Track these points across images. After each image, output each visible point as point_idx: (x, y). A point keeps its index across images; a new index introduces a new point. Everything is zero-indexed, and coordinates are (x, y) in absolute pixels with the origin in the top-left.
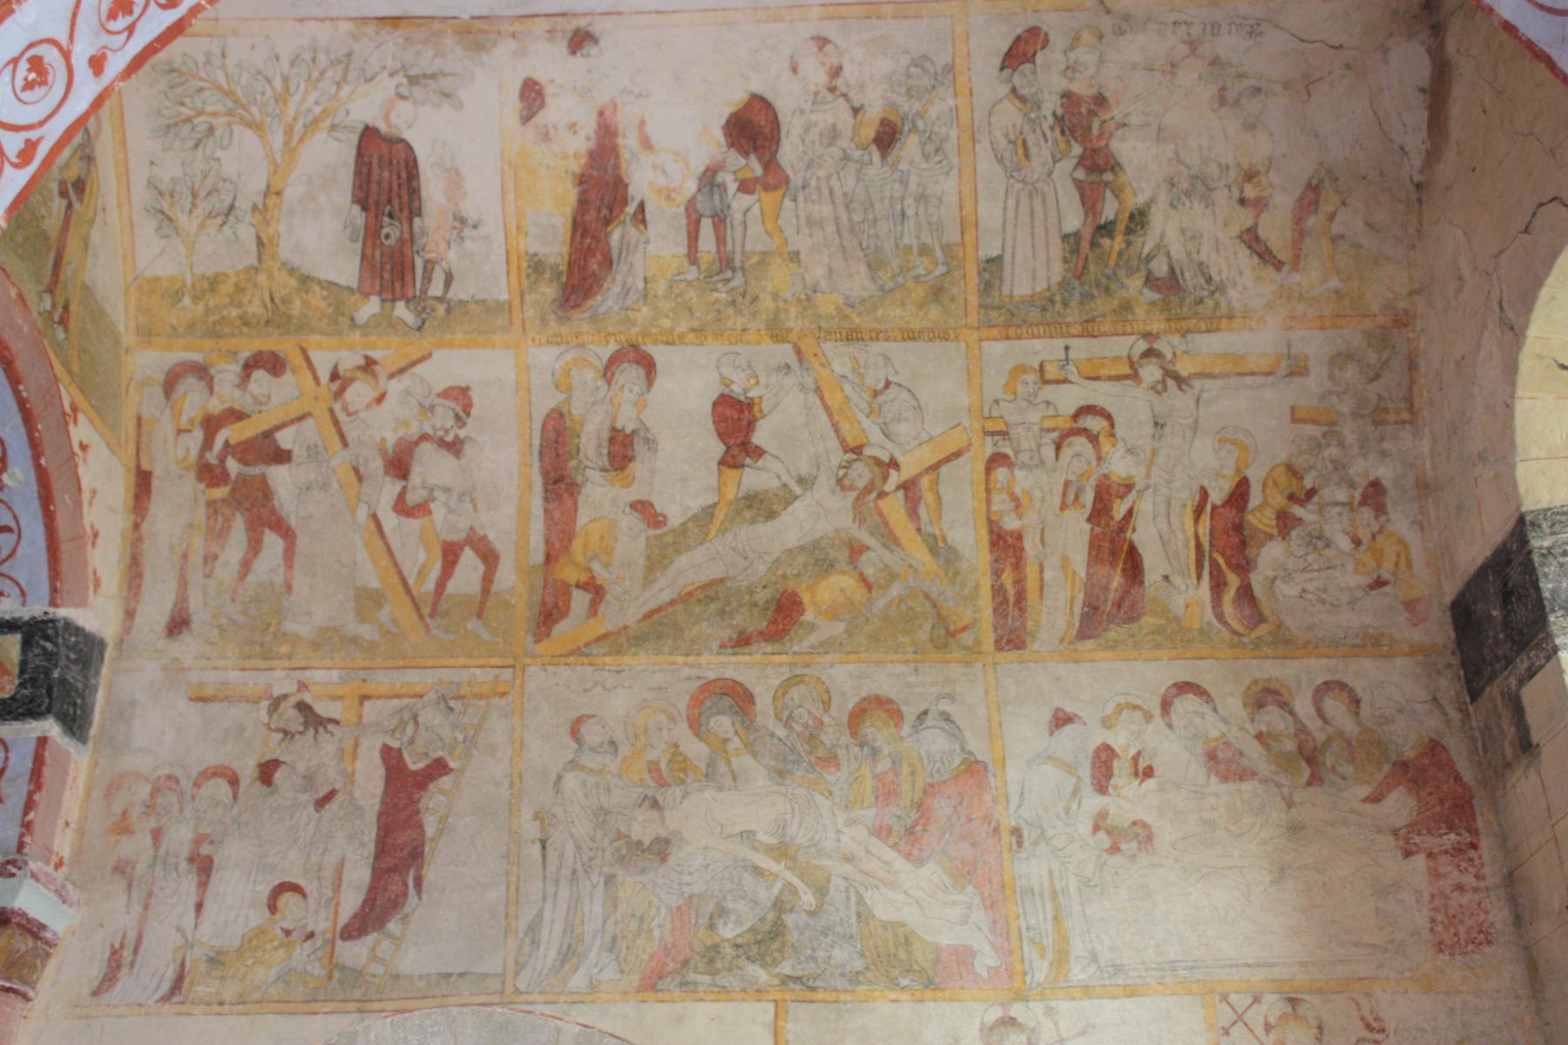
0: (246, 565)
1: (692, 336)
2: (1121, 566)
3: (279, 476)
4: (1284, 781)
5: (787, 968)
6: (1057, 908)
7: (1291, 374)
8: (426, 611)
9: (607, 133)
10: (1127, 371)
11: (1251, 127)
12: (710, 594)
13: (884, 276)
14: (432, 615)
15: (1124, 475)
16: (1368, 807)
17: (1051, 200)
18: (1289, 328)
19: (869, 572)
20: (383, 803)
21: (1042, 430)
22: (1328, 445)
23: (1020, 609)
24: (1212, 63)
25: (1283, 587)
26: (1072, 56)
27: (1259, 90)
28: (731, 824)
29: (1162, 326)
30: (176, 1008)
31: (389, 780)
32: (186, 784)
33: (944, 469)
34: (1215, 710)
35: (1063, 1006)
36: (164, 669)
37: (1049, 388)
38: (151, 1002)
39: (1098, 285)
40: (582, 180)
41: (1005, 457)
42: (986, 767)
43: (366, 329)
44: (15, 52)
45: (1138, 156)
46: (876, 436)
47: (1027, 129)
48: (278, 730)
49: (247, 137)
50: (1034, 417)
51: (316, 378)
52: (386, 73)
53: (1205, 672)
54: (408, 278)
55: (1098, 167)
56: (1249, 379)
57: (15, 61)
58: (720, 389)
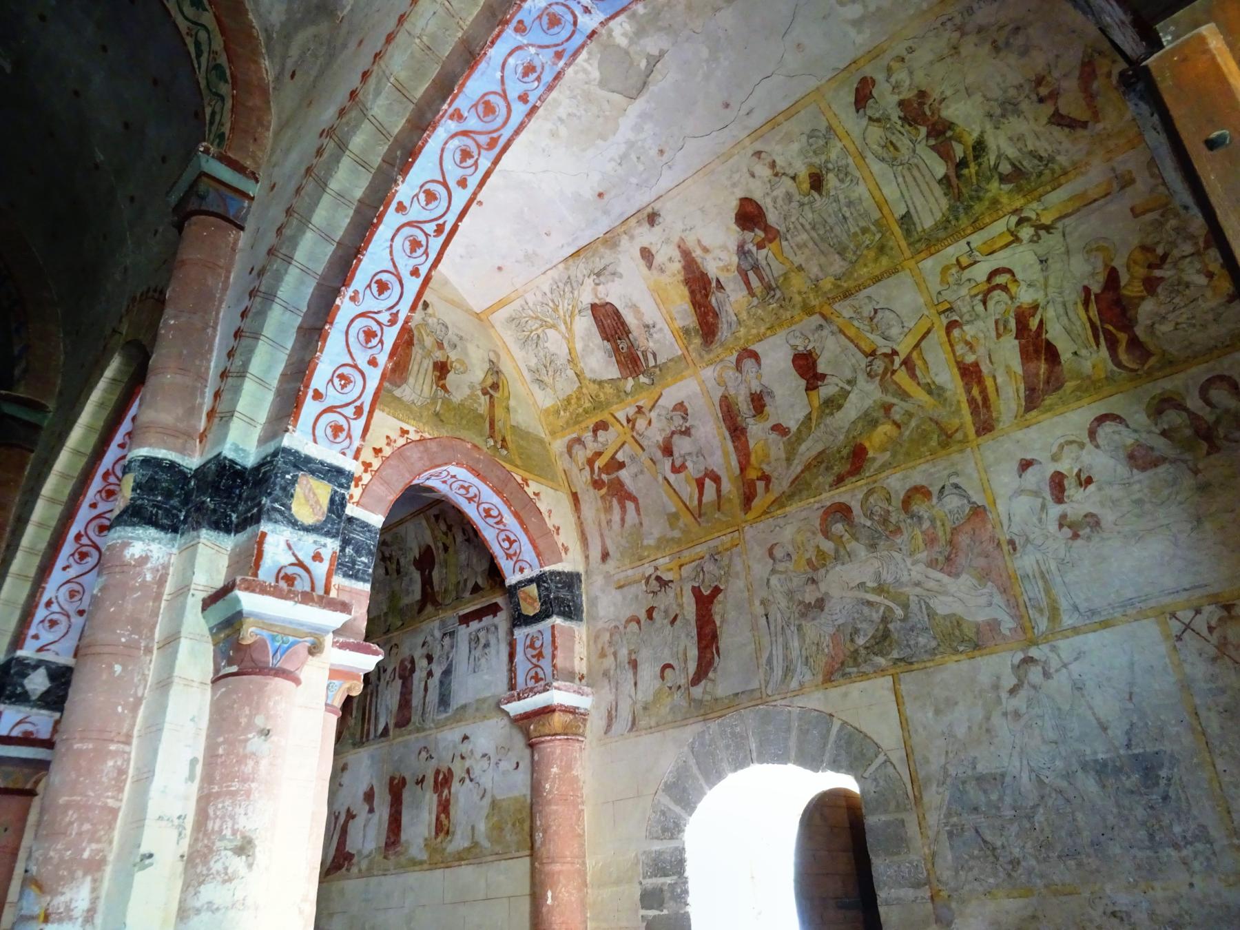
0: (623, 520)
1: (769, 333)
3: (624, 474)
5: (895, 654)
6: (1046, 582)
7: (1123, 188)
9: (686, 255)
11: (1025, 52)
12: (820, 461)
13: (850, 255)
17: (922, 166)
18: (1109, 160)
19: (897, 417)
22: (1168, 220)
24: (979, 32)
26: (893, 80)
28: (853, 575)
33: (923, 344)
35: (1062, 644)
39: (971, 198)
40: (687, 282)
41: (956, 321)
44: (329, 377)
45: (964, 114)
46: (880, 342)
47: (889, 135)
49: (551, 333)
55: (941, 133)
56: (1095, 205)
57: (331, 380)
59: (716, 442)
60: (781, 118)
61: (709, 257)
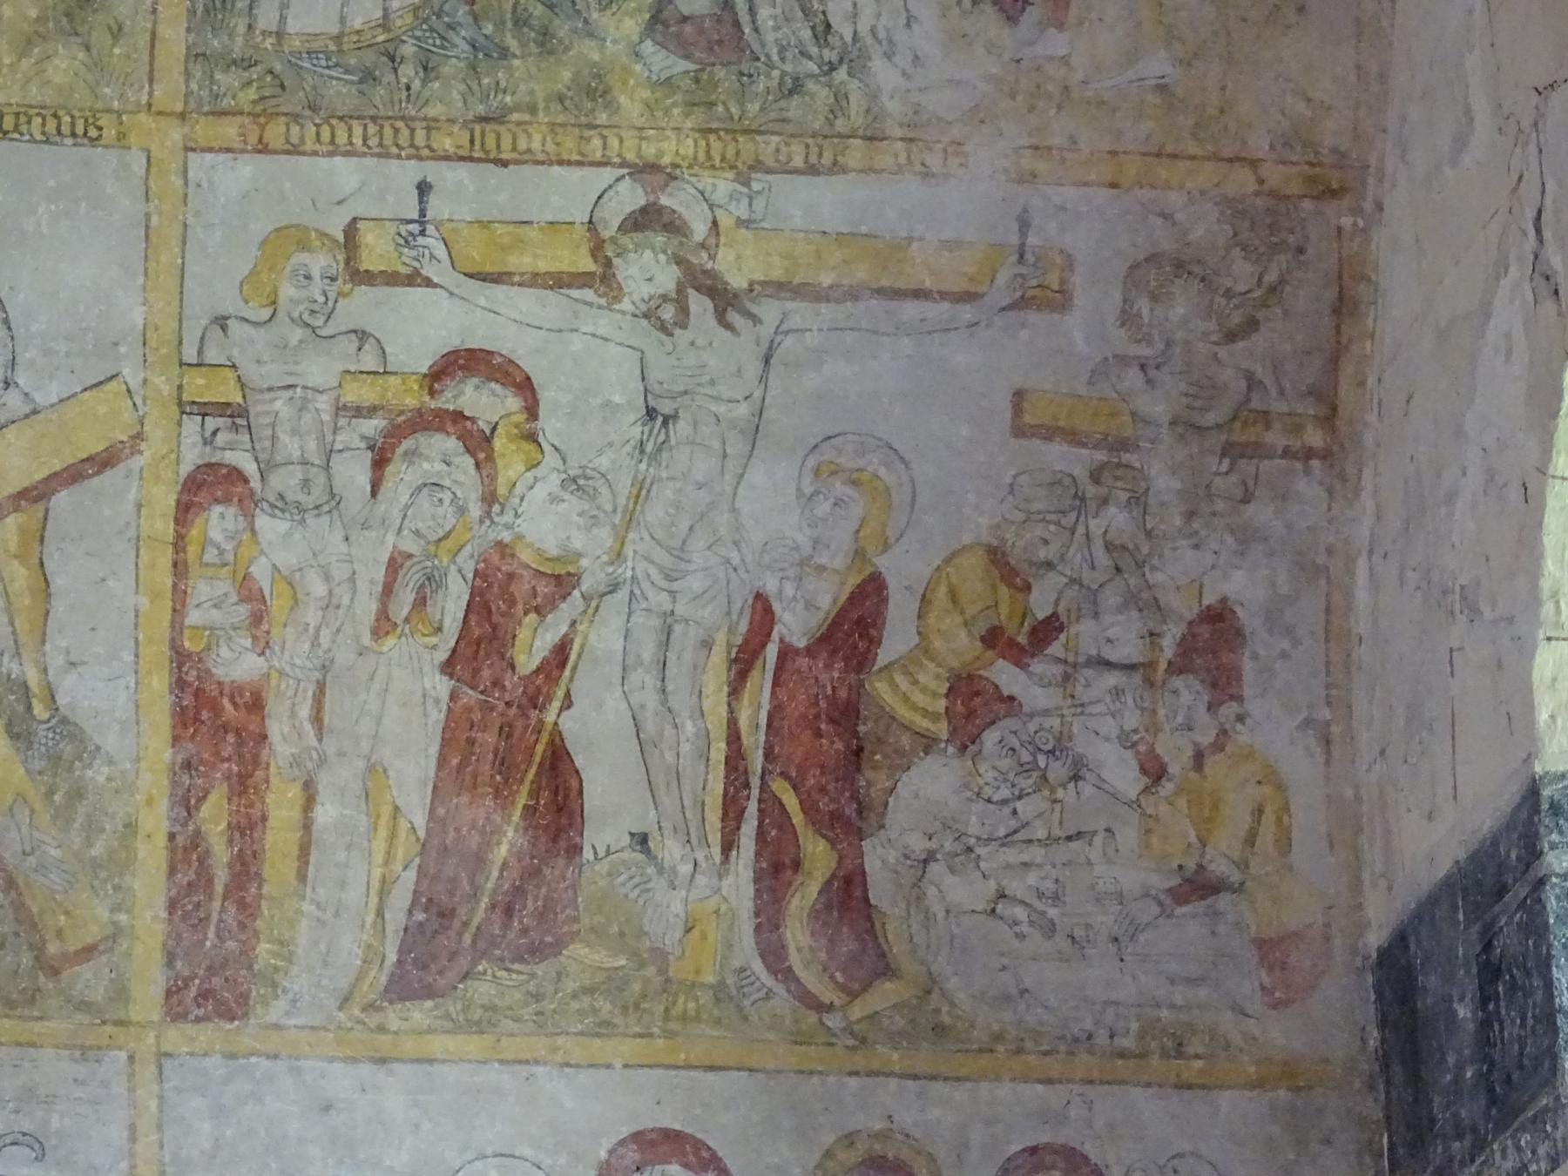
2: (522, 800)
7: (1022, 304)
10: (587, 264)
21: (340, 409)
23: (242, 905)
25: (949, 880)
29: (688, 147)
33: (62, 499)
37: (364, 294)
39: (520, 22)
41: (237, 475)
56: (910, 310)
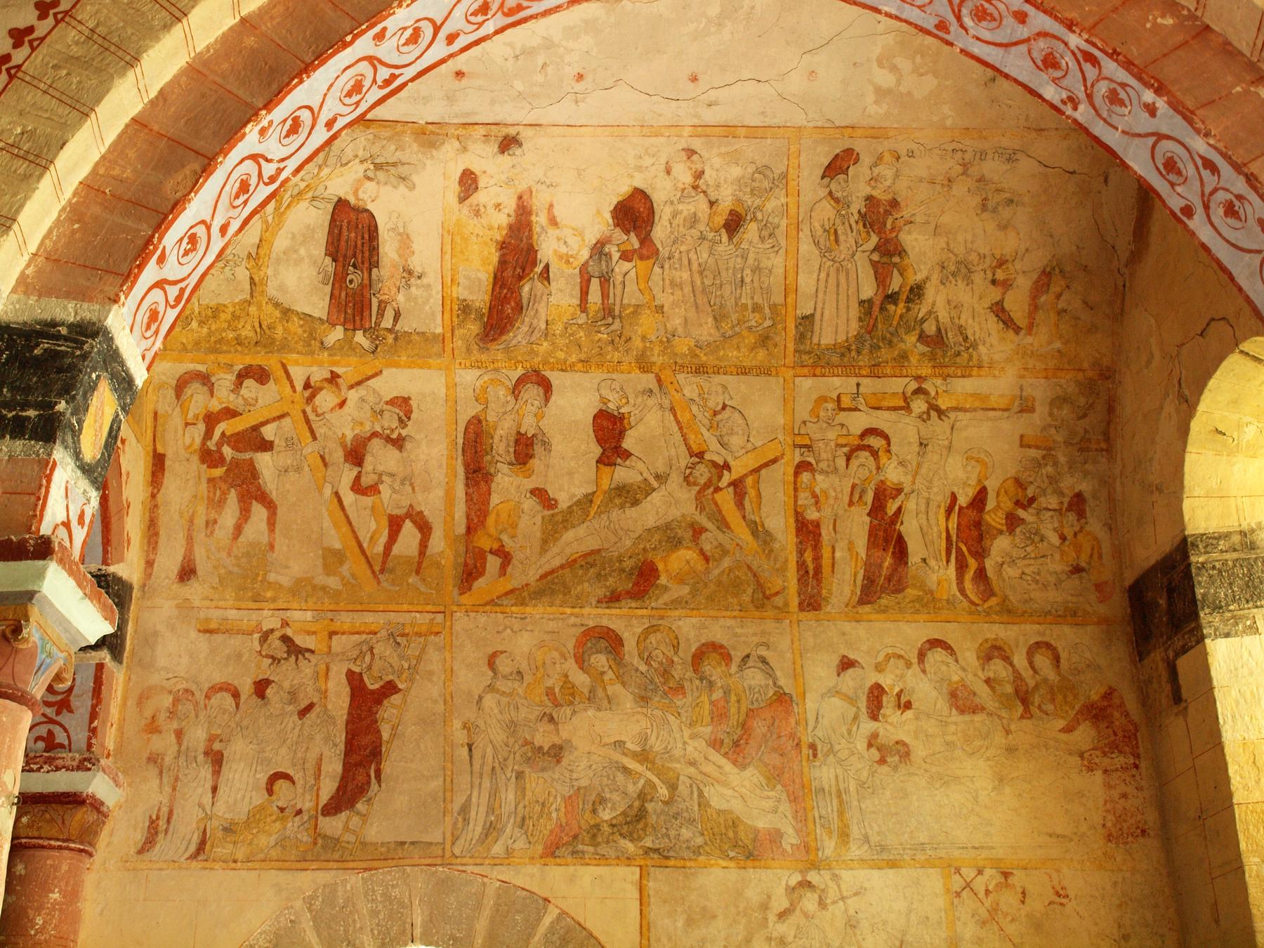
0: (238, 530)
3: (264, 461)
4: (1004, 715)
5: (648, 842)
7: (1021, 411)
8: (377, 568)
10: (902, 404)
12: (589, 561)
14: (382, 571)
15: (896, 481)
16: (1064, 736)
17: (853, 275)
18: (1022, 377)
19: (707, 548)
20: (349, 714)
21: (837, 445)
24: (979, 181)
26: (876, 171)
27: (1012, 201)
28: (607, 732)
29: (929, 371)
30: (201, 865)
31: (353, 696)
32: (199, 696)
33: (763, 472)
34: (957, 661)
35: (846, 875)
36: (178, 606)
38: (182, 859)
39: (884, 339)
40: (503, 246)
41: (810, 464)
42: (791, 698)
43: (331, 350)
46: (714, 445)
47: (838, 221)
48: (267, 656)
50: (831, 435)
51: (293, 387)
52: (357, 161)
53: (950, 633)
54: (366, 313)
55: (889, 254)
56: (992, 413)
58: (599, 406)
59: (439, 475)
60: (743, 132)
61: (553, 232)
